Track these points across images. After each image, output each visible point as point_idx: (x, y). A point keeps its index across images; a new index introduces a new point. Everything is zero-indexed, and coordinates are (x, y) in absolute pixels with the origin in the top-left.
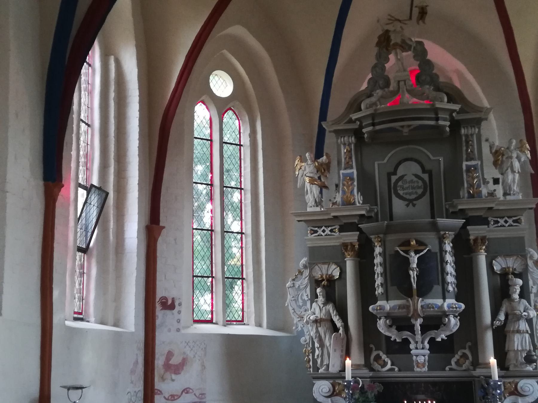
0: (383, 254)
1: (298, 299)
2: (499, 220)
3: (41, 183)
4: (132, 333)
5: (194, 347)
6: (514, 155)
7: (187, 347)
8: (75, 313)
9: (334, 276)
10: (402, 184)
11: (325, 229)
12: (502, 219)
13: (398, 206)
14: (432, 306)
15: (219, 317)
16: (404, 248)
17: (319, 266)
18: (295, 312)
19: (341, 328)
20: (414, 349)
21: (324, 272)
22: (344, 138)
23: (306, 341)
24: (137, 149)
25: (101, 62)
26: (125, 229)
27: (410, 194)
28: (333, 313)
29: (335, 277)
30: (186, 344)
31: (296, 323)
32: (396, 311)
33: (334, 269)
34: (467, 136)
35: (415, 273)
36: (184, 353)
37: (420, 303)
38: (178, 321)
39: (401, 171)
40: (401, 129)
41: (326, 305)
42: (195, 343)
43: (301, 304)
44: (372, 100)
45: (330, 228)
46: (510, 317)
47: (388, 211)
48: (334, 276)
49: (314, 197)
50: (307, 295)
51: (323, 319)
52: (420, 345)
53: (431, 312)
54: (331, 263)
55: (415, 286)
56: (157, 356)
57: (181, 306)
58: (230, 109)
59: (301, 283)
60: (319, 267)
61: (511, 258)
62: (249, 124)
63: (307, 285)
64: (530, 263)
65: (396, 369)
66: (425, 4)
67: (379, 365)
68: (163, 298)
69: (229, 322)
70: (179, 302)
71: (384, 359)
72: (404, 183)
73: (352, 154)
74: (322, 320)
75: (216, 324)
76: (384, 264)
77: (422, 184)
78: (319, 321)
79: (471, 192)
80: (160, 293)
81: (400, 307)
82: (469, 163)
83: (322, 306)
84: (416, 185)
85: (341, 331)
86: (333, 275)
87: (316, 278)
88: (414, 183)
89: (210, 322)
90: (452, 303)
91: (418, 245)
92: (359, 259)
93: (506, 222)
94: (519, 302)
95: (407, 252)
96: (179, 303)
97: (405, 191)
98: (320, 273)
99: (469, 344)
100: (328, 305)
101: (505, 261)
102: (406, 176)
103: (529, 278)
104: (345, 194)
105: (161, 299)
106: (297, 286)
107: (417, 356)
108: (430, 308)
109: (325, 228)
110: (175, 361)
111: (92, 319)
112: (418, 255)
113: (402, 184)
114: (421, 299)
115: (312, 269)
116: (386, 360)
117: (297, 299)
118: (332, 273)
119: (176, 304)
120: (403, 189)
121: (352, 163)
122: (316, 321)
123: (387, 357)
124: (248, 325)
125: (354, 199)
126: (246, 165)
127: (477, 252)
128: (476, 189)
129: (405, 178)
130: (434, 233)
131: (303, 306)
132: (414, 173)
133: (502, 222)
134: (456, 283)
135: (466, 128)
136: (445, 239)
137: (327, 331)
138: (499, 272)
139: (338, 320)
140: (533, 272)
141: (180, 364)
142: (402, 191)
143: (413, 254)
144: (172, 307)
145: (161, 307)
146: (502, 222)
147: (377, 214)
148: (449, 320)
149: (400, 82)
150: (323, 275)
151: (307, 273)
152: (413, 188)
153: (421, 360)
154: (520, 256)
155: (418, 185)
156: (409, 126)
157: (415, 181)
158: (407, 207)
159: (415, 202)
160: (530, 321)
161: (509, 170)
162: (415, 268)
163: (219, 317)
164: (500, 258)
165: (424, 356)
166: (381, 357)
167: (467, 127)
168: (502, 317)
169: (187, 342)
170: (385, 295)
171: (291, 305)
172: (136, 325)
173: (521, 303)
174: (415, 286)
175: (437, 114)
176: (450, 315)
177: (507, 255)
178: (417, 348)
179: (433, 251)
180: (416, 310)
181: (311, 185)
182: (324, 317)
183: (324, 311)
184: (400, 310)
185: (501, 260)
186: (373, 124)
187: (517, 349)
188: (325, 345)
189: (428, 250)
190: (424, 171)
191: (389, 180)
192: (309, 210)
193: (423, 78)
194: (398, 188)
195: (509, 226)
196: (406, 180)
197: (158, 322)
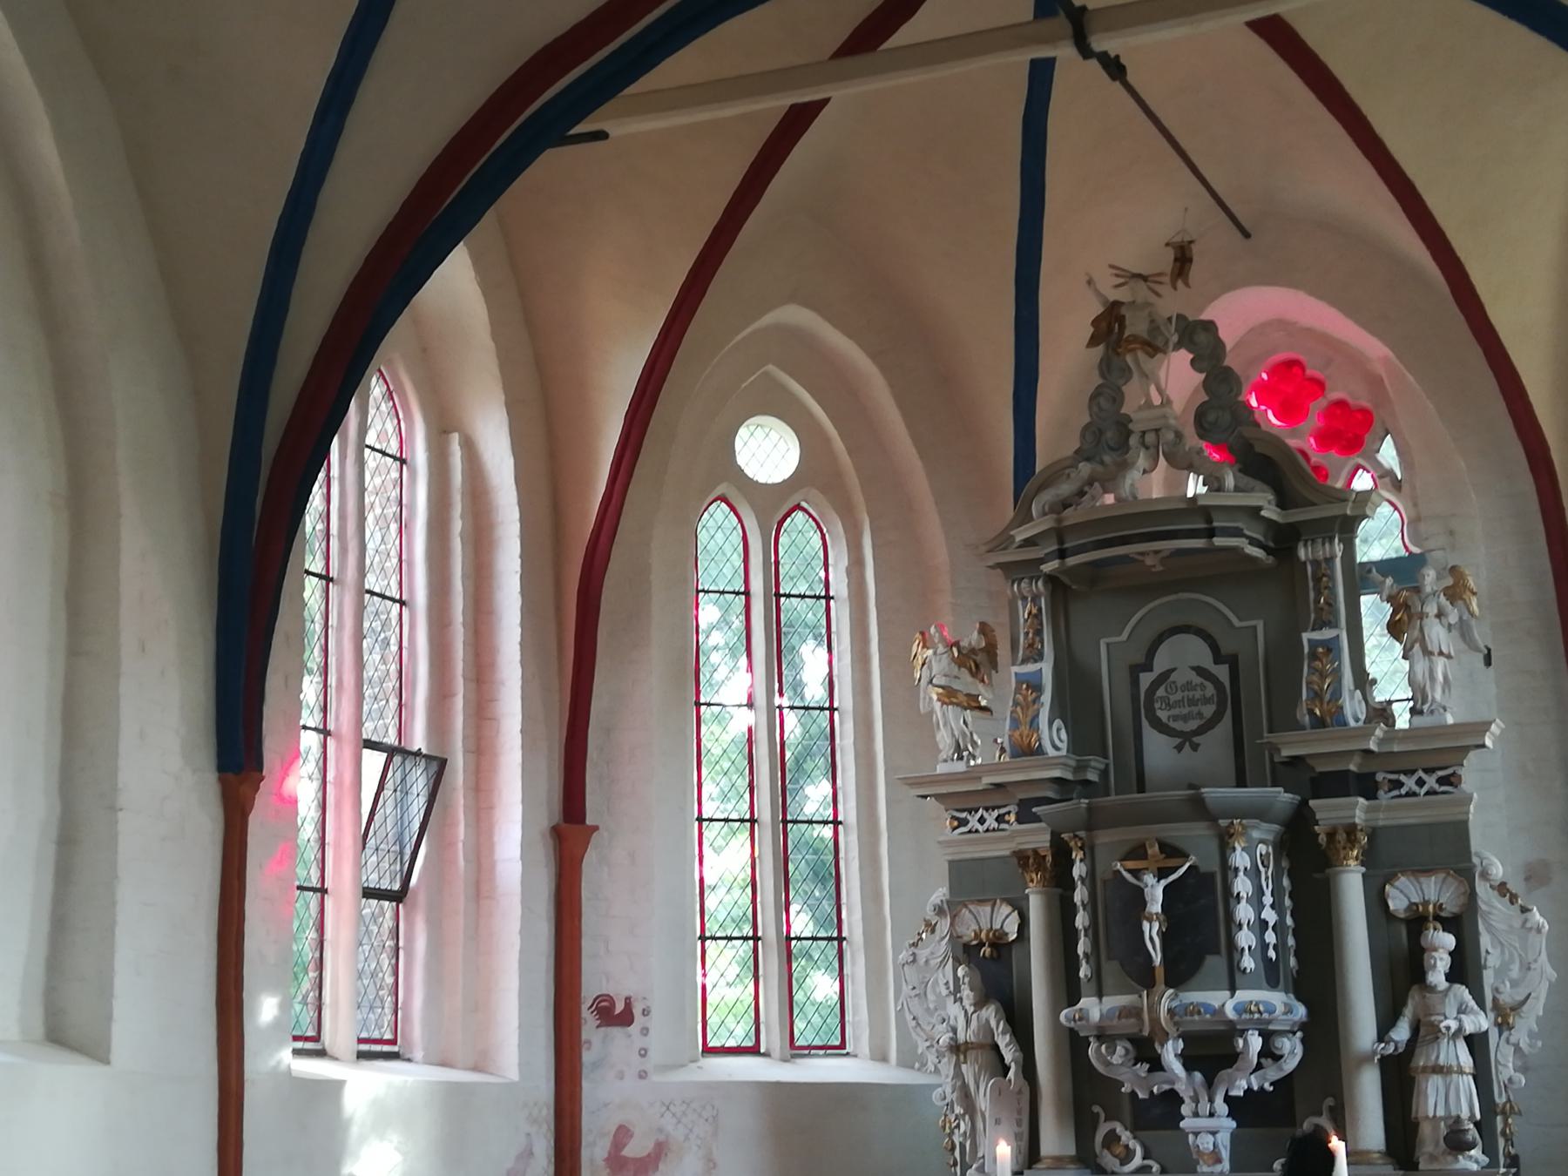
0: (1091, 879)
1: (925, 994)
2: (1402, 778)
3: (211, 778)
4: (510, 1086)
5: (684, 1113)
6: (1432, 609)
7: (668, 1115)
8: (361, 1041)
9: (1007, 934)
10: (1165, 694)
11: (986, 815)
12: (1409, 775)
13: (1158, 750)
14: (1196, 1009)
15: (772, 1038)
16: (1131, 864)
17: (973, 910)
18: (918, 1024)
19: (1013, 1065)
20: (1188, 1117)
21: (985, 925)
22: (1019, 585)
23: (945, 1098)
24: (518, 647)
25: (429, 452)
26: (496, 839)
27: (1185, 718)
28: (997, 1028)
29: (1009, 936)
30: (665, 1108)
31: (922, 1053)
32: (1115, 1022)
33: (1007, 917)
34: (1316, 563)
35: (1156, 926)
36: (660, 1130)
37: (1167, 1000)
38: (643, 1052)
39: (1161, 662)
40: (1140, 558)
41: (981, 1008)
42: (688, 1105)
43: (932, 1006)
44: (1059, 492)
45: (996, 813)
46: (1422, 1032)
47: (1133, 763)
48: (1007, 934)
49: (953, 735)
50: (947, 983)
51: (972, 1043)
52: (1205, 1107)
53: (1195, 1023)
54: (998, 901)
55: (1157, 958)
56: (586, 1138)
57: (649, 1016)
58: (798, 507)
59: (932, 953)
60: (970, 911)
61: (1433, 878)
62: (847, 541)
63: (945, 958)
64: (1481, 888)
65: (1156, 1167)
66: (1187, 239)
67: (1116, 1156)
68: (600, 999)
69: (796, 1050)
70: (644, 1007)
71: (1126, 1143)
72: (1169, 690)
73: (1041, 624)
74: (970, 1046)
75: (766, 1055)
76: (1092, 905)
77: (1214, 692)
78: (962, 1048)
79: (1318, 713)
80: (592, 985)
81: (1125, 1012)
82: (1316, 636)
83: (971, 1009)
84: (1198, 694)
85: (1011, 1074)
86: (1004, 932)
87: (966, 939)
88: (1195, 690)
89: (754, 1050)
90: (1250, 999)
91: (1164, 855)
92: (1059, 891)
93: (1421, 783)
94: (1446, 992)
95: (1136, 873)
96: (644, 1010)
97: (1176, 711)
98: (974, 927)
99: (1330, 1101)
100: (984, 1009)
101: (1417, 884)
102: (1173, 674)
103: (1481, 927)
104: (1018, 728)
105: (597, 1001)
106: (922, 961)
107: (1196, 1134)
108: (1192, 1014)
109: (985, 812)
110: (633, 1150)
111: (418, 1054)
112: (1164, 882)
113: (1165, 694)
114: (1171, 991)
115: (955, 916)
116: (1132, 1144)
117: (922, 992)
118: (1002, 927)
119: (637, 1011)
120: (1169, 706)
121: (1043, 646)
122: (958, 1049)
123: (1135, 1138)
124: (856, 1056)
125: (1039, 739)
126: (842, 648)
127: (1336, 866)
128: (1328, 703)
129: (1173, 677)
130: (1204, 824)
131: (936, 1009)
132: (1196, 664)
133: (1409, 783)
134: (1292, 946)
135: (1309, 543)
136: (1233, 839)
137: (983, 1073)
138: (1402, 916)
139: (1007, 1045)
140: (1489, 913)
141: (649, 1155)
142: (1165, 711)
143: (1149, 879)
144: (626, 1018)
145: (597, 1019)
146: (1409, 783)
147: (1104, 773)
148: (1246, 1041)
149: (1146, 436)
150: (981, 931)
151: (944, 926)
152: (1192, 702)
153: (1206, 1146)
154: (1455, 872)
155: (1204, 695)
156: (1156, 552)
157: (1196, 685)
158: (1179, 751)
159: (1195, 739)
160: (1476, 1044)
161: (1417, 646)
162: (1157, 914)
163: (772, 1038)
164: (1403, 879)
165: (1214, 1133)
166: (1119, 1138)
167: (1313, 541)
168: (1401, 1033)
169: (667, 1104)
170: (1093, 984)
171: (909, 1009)
172: (523, 1065)
173: (1451, 995)
174: (1157, 958)
175: (1209, 521)
176: (1248, 1030)
177: (1421, 870)
178: (1196, 1114)
179: (1203, 868)
180: (1155, 1021)
181: (945, 706)
182: (973, 1039)
183: (974, 1024)
184: (1123, 1020)
185: (1408, 883)
186: (1062, 554)
187: (1435, 1116)
188: (978, 1109)
189: (1189, 867)
190: (1218, 658)
191: (1135, 683)
192: (941, 769)
193: (1211, 417)
194: (1157, 705)
195: (1427, 793)
196: (1174, 682)
197: (587, 1057)
